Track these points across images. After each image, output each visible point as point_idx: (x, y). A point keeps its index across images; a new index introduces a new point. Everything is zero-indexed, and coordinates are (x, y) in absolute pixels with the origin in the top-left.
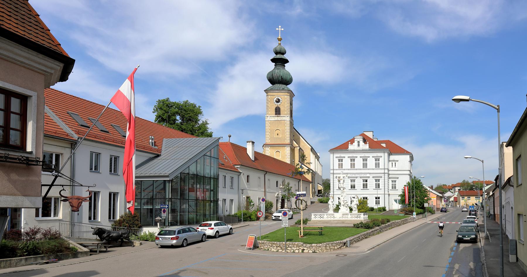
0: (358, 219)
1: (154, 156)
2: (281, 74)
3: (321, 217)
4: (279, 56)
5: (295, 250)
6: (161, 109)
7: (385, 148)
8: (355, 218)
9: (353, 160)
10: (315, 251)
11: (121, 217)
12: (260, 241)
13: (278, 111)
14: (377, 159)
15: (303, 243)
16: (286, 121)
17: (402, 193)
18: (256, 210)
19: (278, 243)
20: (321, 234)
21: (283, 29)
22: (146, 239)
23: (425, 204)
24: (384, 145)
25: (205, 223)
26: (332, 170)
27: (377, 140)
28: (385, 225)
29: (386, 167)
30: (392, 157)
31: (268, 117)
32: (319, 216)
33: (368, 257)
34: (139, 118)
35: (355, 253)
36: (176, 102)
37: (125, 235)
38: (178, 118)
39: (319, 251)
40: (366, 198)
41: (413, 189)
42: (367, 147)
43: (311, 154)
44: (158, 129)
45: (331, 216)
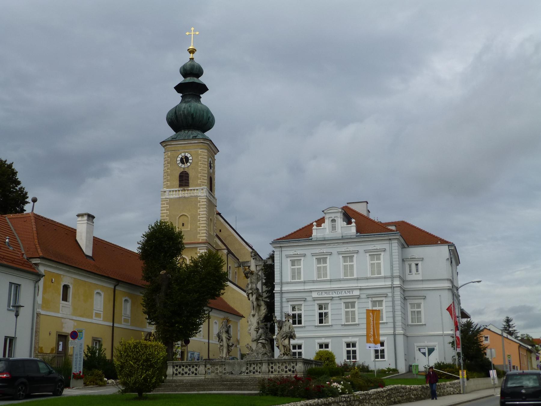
2: (191, 110)
4: (189, 80)
24: (393, 228)
31: (165, 191)
42: (352, 229)
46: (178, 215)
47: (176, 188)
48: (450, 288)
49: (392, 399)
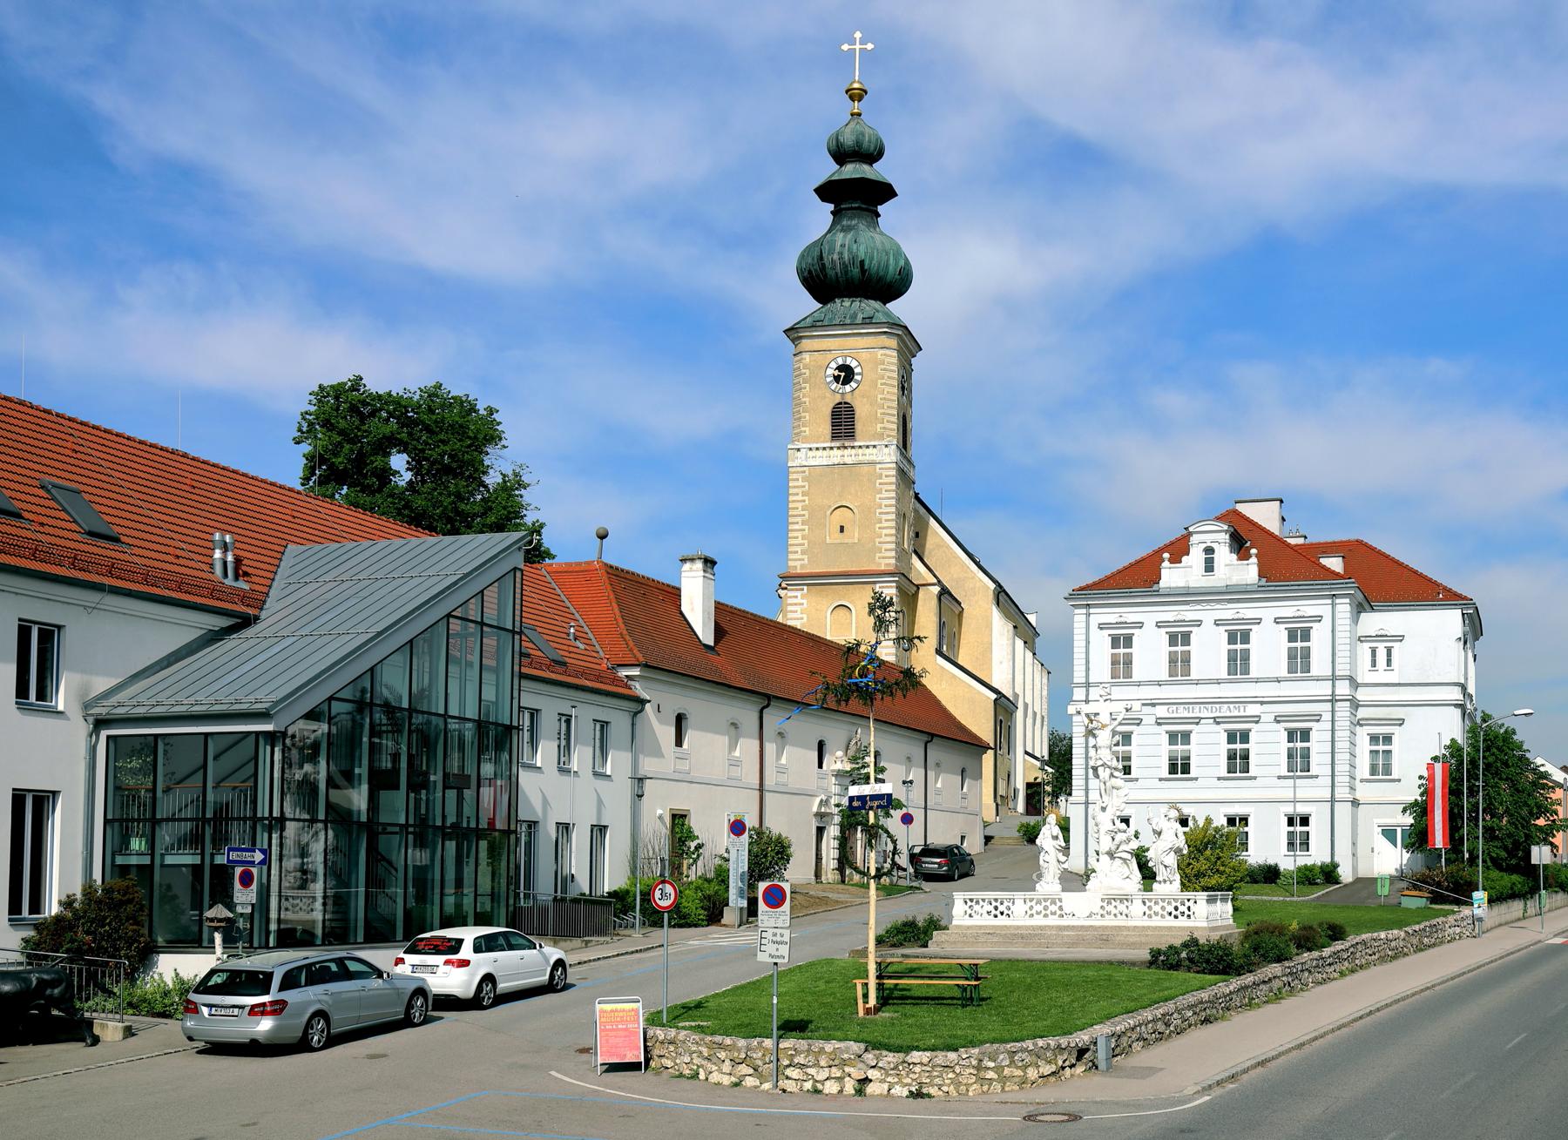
0: (1182, 922)
1: (224, 622)
3: (998, 913)
4: (851, 171)
5: (822, 1082)
6: (327, 424)
7: (1337, 574)
8: (1162, 916)
9: (1180, 638)
10: (925, 1091)
11: (68, 903)
12: (658, 1032)
13: (843, 423)
14: (1298, 634)
15: (862, 1046)
16: (879, 466)
17: (1422, 795)
18: (711, 875)
19: (742, 1043)
20: (968, 999)
21: (870, 46)
22: (159, 1008)
23: (1535, 850)
24: (1335, 563)
25: (433, 938)
26: (1079, 685)
27: (1301, 541)
28: (1315, 954)
29: (1342, 670)
30: (1374, 622)
31: (799, 450)
32: (991, 908)
33: (1191, 1131)
34: (185, 455)
35: (1127, 1105)
36: (389, 394)
37: (56, 991)
38: (399, 461)
39: (945, 1089)
40: (1244, 820)
41: (1473, 776)
42: (1249, 572)
43: (996, 614)
44: (268, 506)
45: (1046, 908)
46: (830, 507)
47: (823, 442)
48: (1460, 702)
49: (1357, 961)
